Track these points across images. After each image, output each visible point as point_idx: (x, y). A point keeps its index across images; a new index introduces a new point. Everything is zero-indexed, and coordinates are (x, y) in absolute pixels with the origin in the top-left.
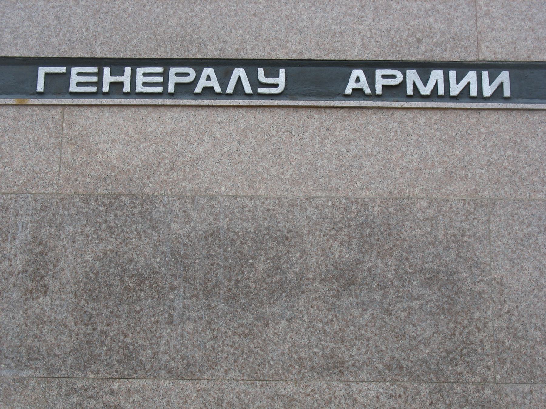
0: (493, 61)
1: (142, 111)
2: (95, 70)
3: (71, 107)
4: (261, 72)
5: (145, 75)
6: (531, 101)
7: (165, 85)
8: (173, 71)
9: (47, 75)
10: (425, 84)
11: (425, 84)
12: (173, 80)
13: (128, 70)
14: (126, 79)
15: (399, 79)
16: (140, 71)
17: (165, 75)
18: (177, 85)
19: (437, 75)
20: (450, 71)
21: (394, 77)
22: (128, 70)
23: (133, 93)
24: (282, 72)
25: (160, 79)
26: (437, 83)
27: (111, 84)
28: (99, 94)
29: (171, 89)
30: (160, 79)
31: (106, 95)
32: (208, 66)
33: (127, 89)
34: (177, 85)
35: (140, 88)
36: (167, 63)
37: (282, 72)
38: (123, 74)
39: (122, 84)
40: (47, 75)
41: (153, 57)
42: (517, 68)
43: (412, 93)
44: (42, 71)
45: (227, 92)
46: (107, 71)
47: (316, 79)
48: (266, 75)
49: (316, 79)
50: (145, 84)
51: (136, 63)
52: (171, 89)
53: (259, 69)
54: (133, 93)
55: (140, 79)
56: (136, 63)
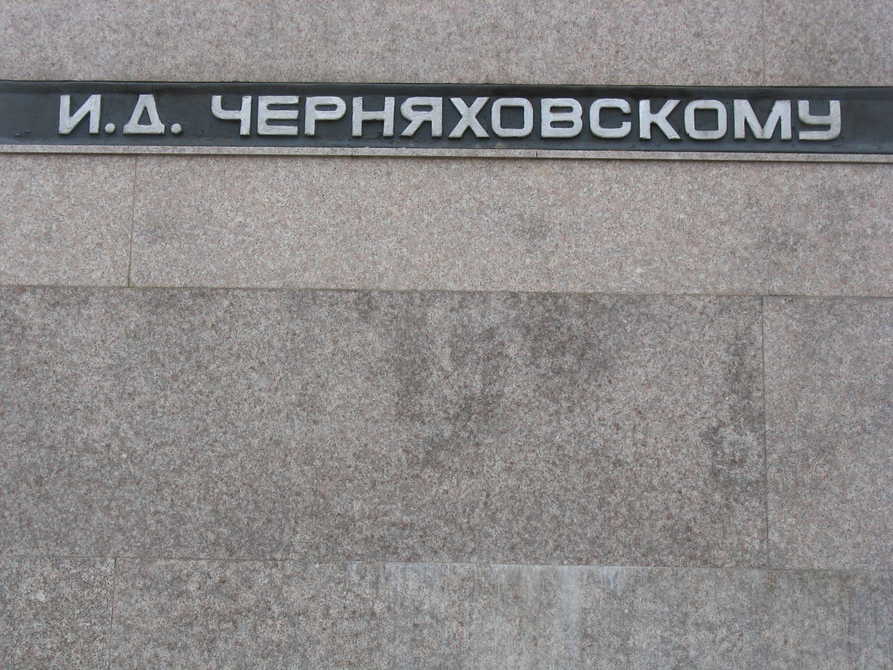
1: (655, 168)
2: (295, 100)
4: (804, 106)
7: (300, 122)
8: (312, 102)
10: (763, 123)
11: (763, 123)
12: (313, 115)
13: (247, 101)
14: (387, 114)
16: (264, 102)
17: (300, 107)
18: (318, 122)
19: (781, 109)
21: (333, 107)
22: (247, 101)
23: (254, 137)
24: (835, 106)
25: (293, 114)
26: (746, 123)
28: (301, 138)
29: (310, 129)
30: (293, 114)
31: (313, 140)
32: (780, 99)
35: (263, 129)
36: (304, 90)
37: (835, 106)
38: (239, 108)
40: (697, 111)
41: (796, 85)
42: (856, 100)
45: (452, 135)
46: (357, 102)
47: (194, 112)
48: (812, 112)
49: (194, 112)
50: (554, 124)
51: (257, 90)
52: (310, 129)
53: (386, 99)
54: (254, 137)
55: (264, 114)
56: (257, 90)
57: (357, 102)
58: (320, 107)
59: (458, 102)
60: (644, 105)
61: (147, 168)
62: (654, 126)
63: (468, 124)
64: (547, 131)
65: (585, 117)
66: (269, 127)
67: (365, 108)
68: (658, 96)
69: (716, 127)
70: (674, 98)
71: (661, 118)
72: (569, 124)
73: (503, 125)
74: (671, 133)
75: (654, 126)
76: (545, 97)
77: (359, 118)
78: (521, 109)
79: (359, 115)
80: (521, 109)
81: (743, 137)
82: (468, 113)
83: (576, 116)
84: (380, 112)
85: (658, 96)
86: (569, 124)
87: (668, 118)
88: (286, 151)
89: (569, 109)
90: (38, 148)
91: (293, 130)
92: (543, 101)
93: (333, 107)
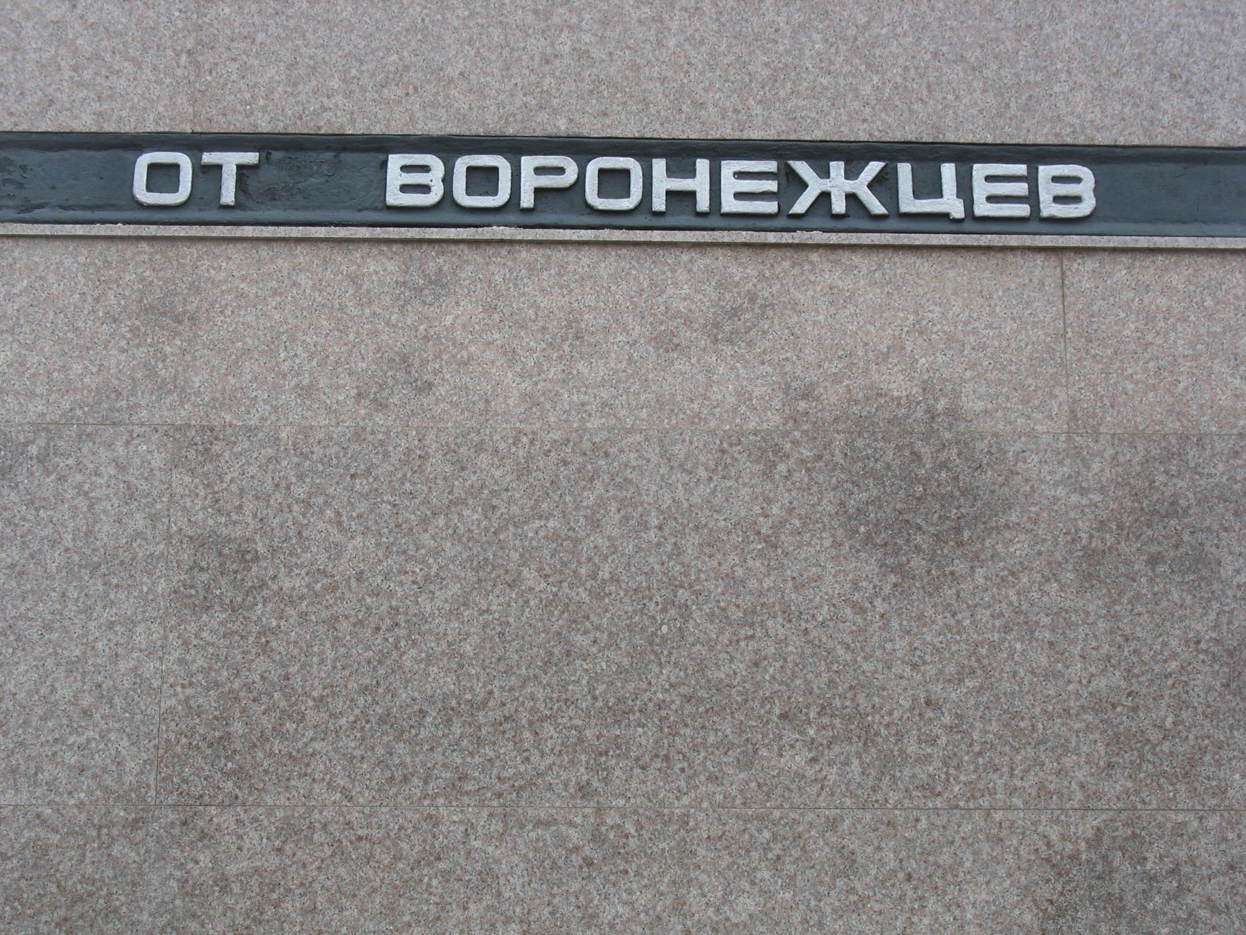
0: (1233, 149)
2: (1021, 169)
3: (275, 245)
5: (405, 169)
6: (1186, 228)
7: (1032, 198)
9: (470, 170)
13: (703, 165)
14: (700, 184)
15: (570, 176)
16: (729, 168)
18: (539, 192)
20: (523, 158)
21: (560, 171)
22: (703, 165)
25: (1021, 189)
27: (669, 193)
30: (1021, 189)
33: (703, 203)
34: (539, 192)
35: (729, 204)
39: (692, 195)
40: (470, 170)
43: (663, 208)
44: (395, 161)
46: (659, 166)
47: (310, 178)
49: (310, 178)
50: (405, 188)
51: (719, 151)
55: (730, 185)
56: (719, 151)
57: (659, 166)
58: (539, 171)
59: (802, 168)
60: (837, 168)
61: (1083, 271)
62: (851, 198)
63: (945, 199)
64: (729, 204)
65: (448, 180)
66: (990, 205)
67: (671, 172)
68: (854, 155)
69: (627, 194)
70: (879, 160)
71: (815, 185)
72: (425, 189)
73: (469, 191)
74: (877, 207)
75: (851, 198)
76: (393, 153)
77: (594, 189)
78: (495, 170)
79: (663, 182)
80: (495, 170)
81: (962, 215)
82: (838, 183)
83: (435, 177)
84: (689, 181)
85: (854, 155)
86: (425, 189)
87: (804, 186)
88: (1013, 240)
89: (425, 169)
90: (119, 230)
91: (1023, 210)
92: (976, 166)
93: (560, 171)
